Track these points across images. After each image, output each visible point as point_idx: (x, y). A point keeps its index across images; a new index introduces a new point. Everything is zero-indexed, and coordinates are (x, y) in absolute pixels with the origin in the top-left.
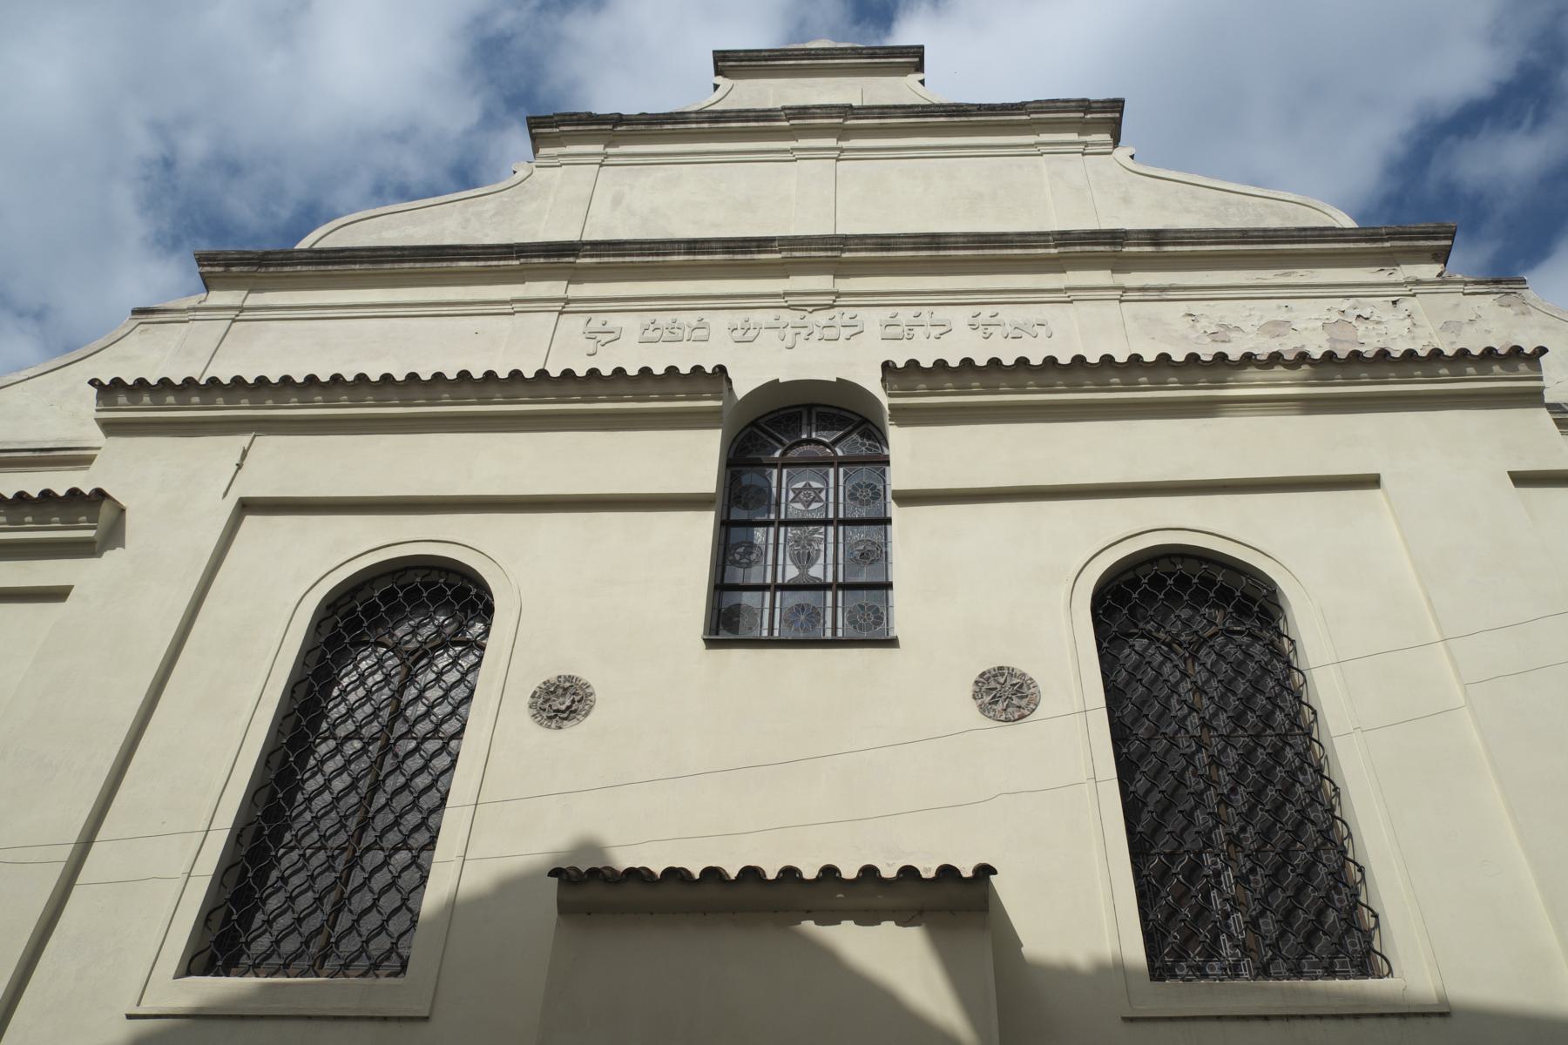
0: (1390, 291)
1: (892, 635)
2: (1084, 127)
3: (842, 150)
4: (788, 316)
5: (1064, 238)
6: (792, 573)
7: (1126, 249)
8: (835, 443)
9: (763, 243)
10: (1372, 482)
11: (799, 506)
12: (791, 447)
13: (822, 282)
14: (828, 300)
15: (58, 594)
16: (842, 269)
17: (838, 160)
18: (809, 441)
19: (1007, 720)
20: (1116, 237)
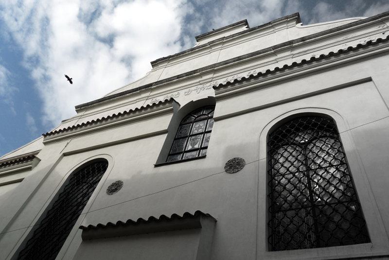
0: (382, 31)
1: (42, 76)
2: (288, 22)
3: (293, 55)
4: (200, 86)
5: (275, 47)
6: (190, 147)
7: (294, 45)
8: (209, 114)
9: (195, 72)
10: (369, 80)
11: (196, 131)
12: (197, 117)
13: (211, 76)
14: (210, 80)
15: (20, 181)
16: (215, 72)
17: (292, 58)
18: (203, 115)
19: (233, 173)
20: (291, 42)
